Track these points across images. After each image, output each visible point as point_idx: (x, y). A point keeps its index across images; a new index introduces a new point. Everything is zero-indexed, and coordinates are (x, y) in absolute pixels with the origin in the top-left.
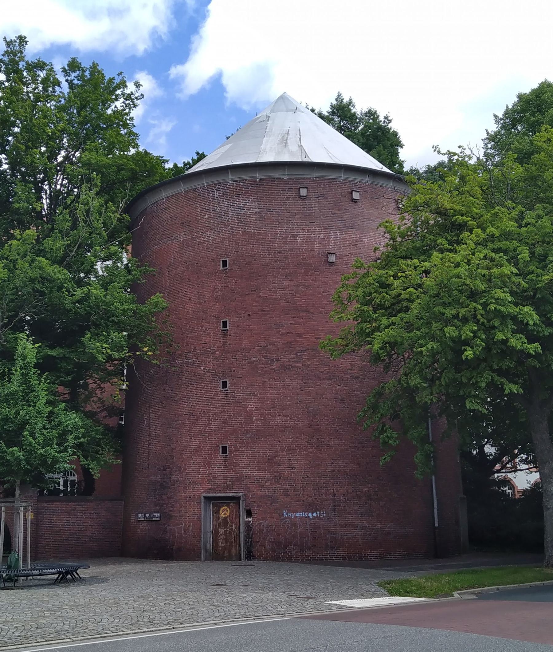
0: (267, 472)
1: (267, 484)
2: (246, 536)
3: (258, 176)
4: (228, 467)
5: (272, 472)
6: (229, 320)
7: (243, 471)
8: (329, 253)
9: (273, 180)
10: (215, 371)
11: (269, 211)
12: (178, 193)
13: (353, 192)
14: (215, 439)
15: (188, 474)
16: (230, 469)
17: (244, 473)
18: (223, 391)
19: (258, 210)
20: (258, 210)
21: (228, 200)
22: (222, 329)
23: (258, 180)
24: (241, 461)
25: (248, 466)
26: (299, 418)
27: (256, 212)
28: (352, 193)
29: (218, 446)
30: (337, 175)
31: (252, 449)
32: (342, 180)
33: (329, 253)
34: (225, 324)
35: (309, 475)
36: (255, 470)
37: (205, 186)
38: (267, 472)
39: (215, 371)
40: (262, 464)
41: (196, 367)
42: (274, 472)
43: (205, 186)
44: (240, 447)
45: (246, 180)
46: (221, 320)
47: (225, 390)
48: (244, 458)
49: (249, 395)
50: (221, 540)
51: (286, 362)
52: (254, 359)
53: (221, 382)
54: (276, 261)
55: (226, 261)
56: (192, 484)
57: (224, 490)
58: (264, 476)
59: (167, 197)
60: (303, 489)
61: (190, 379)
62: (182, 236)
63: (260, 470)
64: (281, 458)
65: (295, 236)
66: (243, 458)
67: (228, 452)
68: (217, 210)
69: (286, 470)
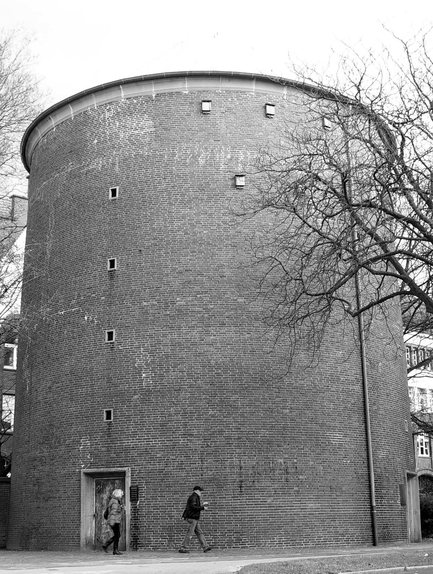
0: (159, 441)
1: (158, 455)
2: (131, 520)
3: (153, 90)
4: (113, 436)
5: (164, 441)
6: (117, 258)
7: (130, 440)
8: (237, 176)
9: (171, 94)
10: (100, 320)
11: (165, 129)
12: (68, 120)
13: (267, 106)
14: (99, 402)
15: (68, 446)
16: (115, 438)
17: (131, 442)
18: (108, 343)
19: (154, 129)
20: (154, 129)
21: (120, 121)
22: (109, 269)
23: (154, 96)
24: (128, 428)
25: (135, 434)
26: (198, 373)
27: (151, 132)
28: (265, 108)
29: (102, 411)
30: (246, 87)
31: (141, 412)
32: (253, 94)
33: (237, 176)
34: (112, 263)
35: (209, 443)
36: (144, 439)
37: (96, 108)
38: (159, 441)
39: (100, 320)
40: (152, 431)
41: (79, 317)
42: (167, 441)
43: (96, 108)
44: (126, 411)
45: (141, 97)
46: (109, 259)
47: (111, 343)
48: (131, 425)
49: (139, 348)
50: (105, 525)
51: (184, 305)
52: (145, 304)
53: (106, 333)
54: (173, 187)
55: (115, 189)
56: (72, 458)
57: (372, 417)
58: (154, 446)
59: (57, 126)
60: (202, 461)
61: (73, 332)
62: (70, 167)
63: (150, 439)
64: (175, 423)
65: (195, 158)
66: (130, 425)
67: (112, 418)
68: (108, 133)
69: (181, 437)
